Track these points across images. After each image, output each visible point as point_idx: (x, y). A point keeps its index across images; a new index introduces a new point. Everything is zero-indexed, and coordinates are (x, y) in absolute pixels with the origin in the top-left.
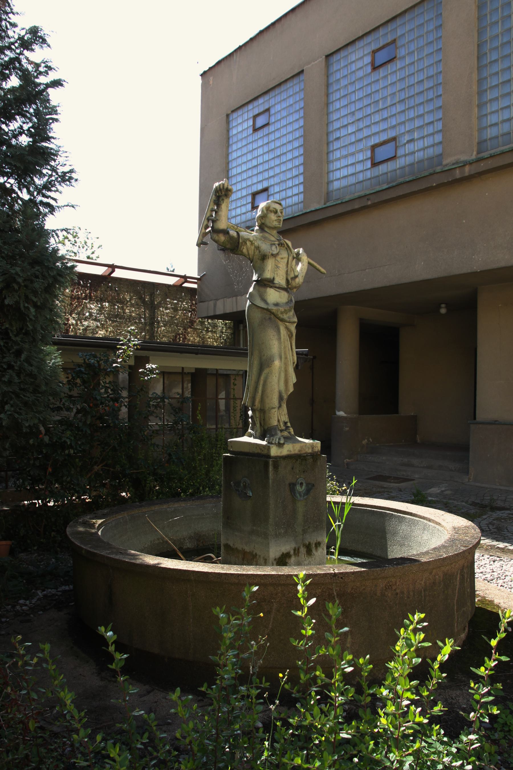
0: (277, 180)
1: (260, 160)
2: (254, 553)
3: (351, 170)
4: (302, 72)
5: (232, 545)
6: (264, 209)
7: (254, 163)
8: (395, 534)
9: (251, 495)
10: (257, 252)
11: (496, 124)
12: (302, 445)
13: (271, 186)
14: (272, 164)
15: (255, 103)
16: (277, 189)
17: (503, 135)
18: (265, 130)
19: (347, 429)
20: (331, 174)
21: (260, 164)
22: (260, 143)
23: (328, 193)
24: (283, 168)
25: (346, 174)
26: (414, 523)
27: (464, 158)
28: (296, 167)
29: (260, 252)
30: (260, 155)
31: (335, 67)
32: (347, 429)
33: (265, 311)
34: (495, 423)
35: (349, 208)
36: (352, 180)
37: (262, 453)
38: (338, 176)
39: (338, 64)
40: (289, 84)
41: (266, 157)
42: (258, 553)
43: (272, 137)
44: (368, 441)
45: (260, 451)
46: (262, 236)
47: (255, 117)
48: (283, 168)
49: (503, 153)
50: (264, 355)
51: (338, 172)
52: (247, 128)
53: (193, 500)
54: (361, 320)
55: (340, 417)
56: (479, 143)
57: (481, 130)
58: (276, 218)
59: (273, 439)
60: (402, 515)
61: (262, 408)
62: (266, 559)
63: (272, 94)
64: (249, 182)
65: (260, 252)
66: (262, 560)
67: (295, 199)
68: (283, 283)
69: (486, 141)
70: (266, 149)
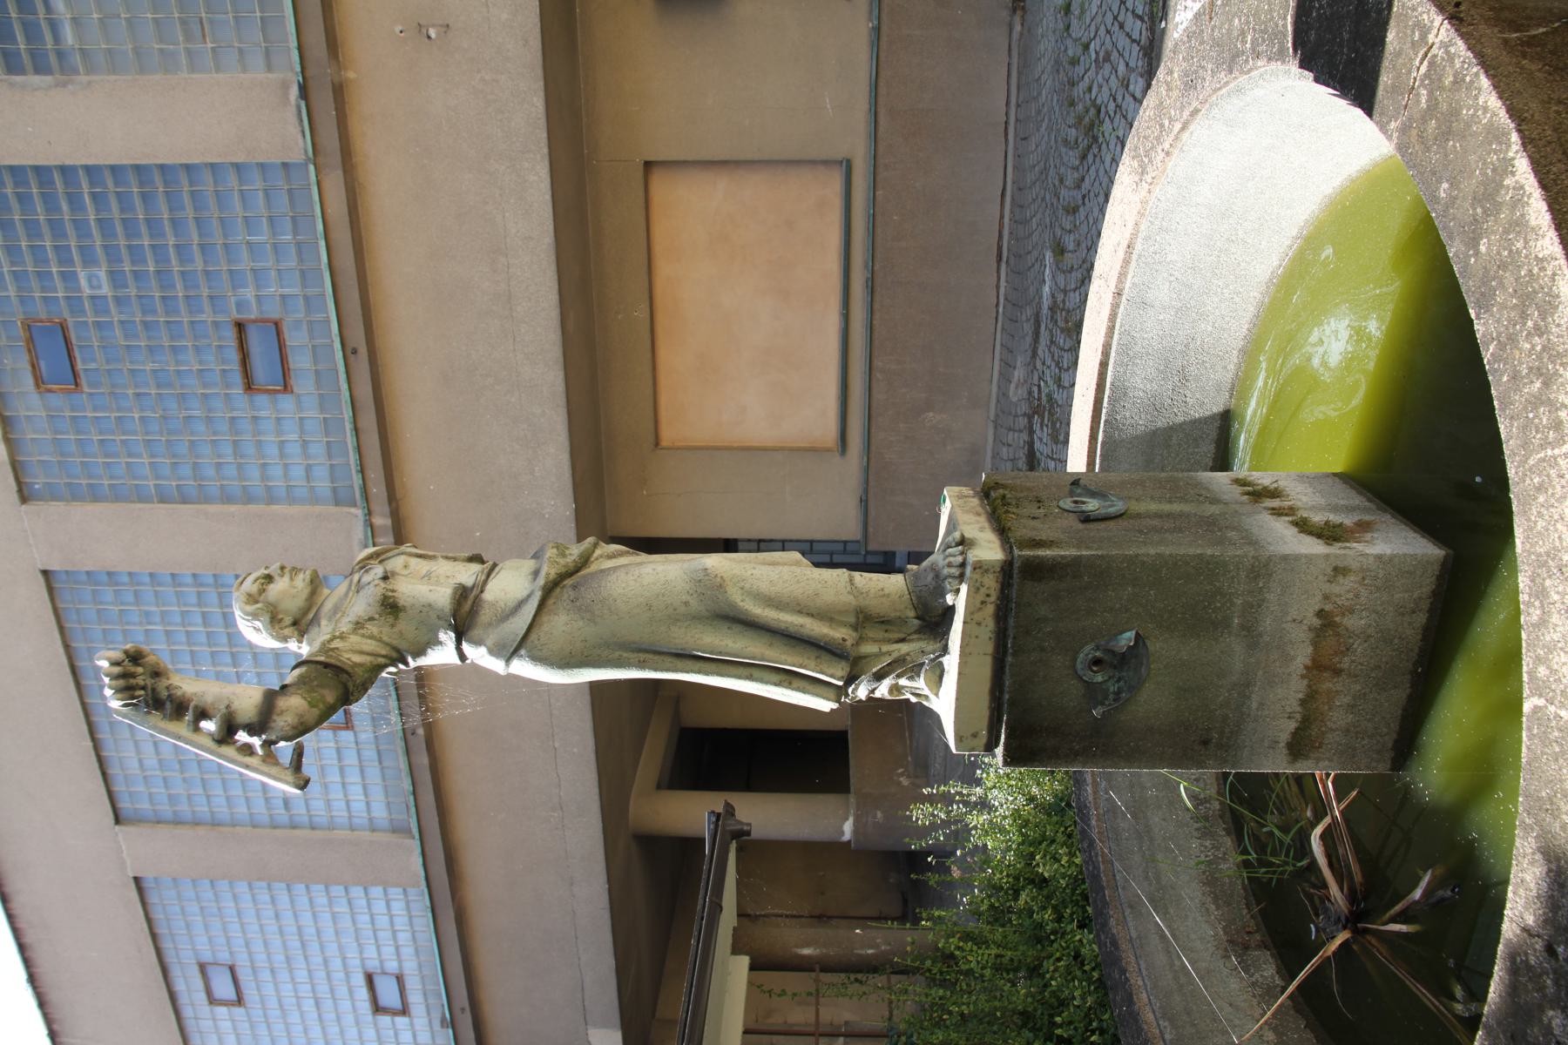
0: (352, 953)
1: (305, 990)
2: (1317, 622)
3: (354, 777)
4: (137, 880)
5: (1293, 725)
6: (250, 608)
7: (309, 1005)
8: (1156, 408)
9: (1130, 635)
10: (372, 628)
11: (308, 468)
12: (957, 510)
13: (363, 965)
14: (317, 960)
15: (183, 1000)
16: (371, 952)
17: (330, 457)
18: (245, 976)
19: (879, 814)
20: (355, 820)
21: (313, 991)
22: (269, 989)
23: (394, 831)
24: (329, 933)
25: (359, 789)
26: (1125, 350)
27: (359, 531)
28: (330, 904)
29: (371, 619)
30: (296, 991)
31: (145, 805)
32: (879, 814)
33: (551, 601)
34: (864, 502)
35: (426, 777)
36: (374, 773)
37: (993, 598)
38: (362, 806)
39: (135, 798)
40: (158, 915)
41: (302, 975)
42: (1315, 604)
43: (261, 958)
44: (902, 774)
45: (990, 609)
46: (330, 620)
47: (212, 1000)
48: (329, 933)
49: (359, 449)
50: (686, 603)
51: (353, 804)
52: (233, 1021)
53: (1123, 971)
54: (659, 787)
55: (856, 831)
56: (338, 503)
57: (314, 499)
58: (286, 578)
59: (950, 565)
60: (1107, 392)
61: (852, 620)
62: (1336, 569)
63: (170, 958)
64: (349, 1019)
65: (371, 619)
66: (1336, 589)
67: (398, 907)
68: (328, 493)
69: (334, 490)
70: (284, 976)
